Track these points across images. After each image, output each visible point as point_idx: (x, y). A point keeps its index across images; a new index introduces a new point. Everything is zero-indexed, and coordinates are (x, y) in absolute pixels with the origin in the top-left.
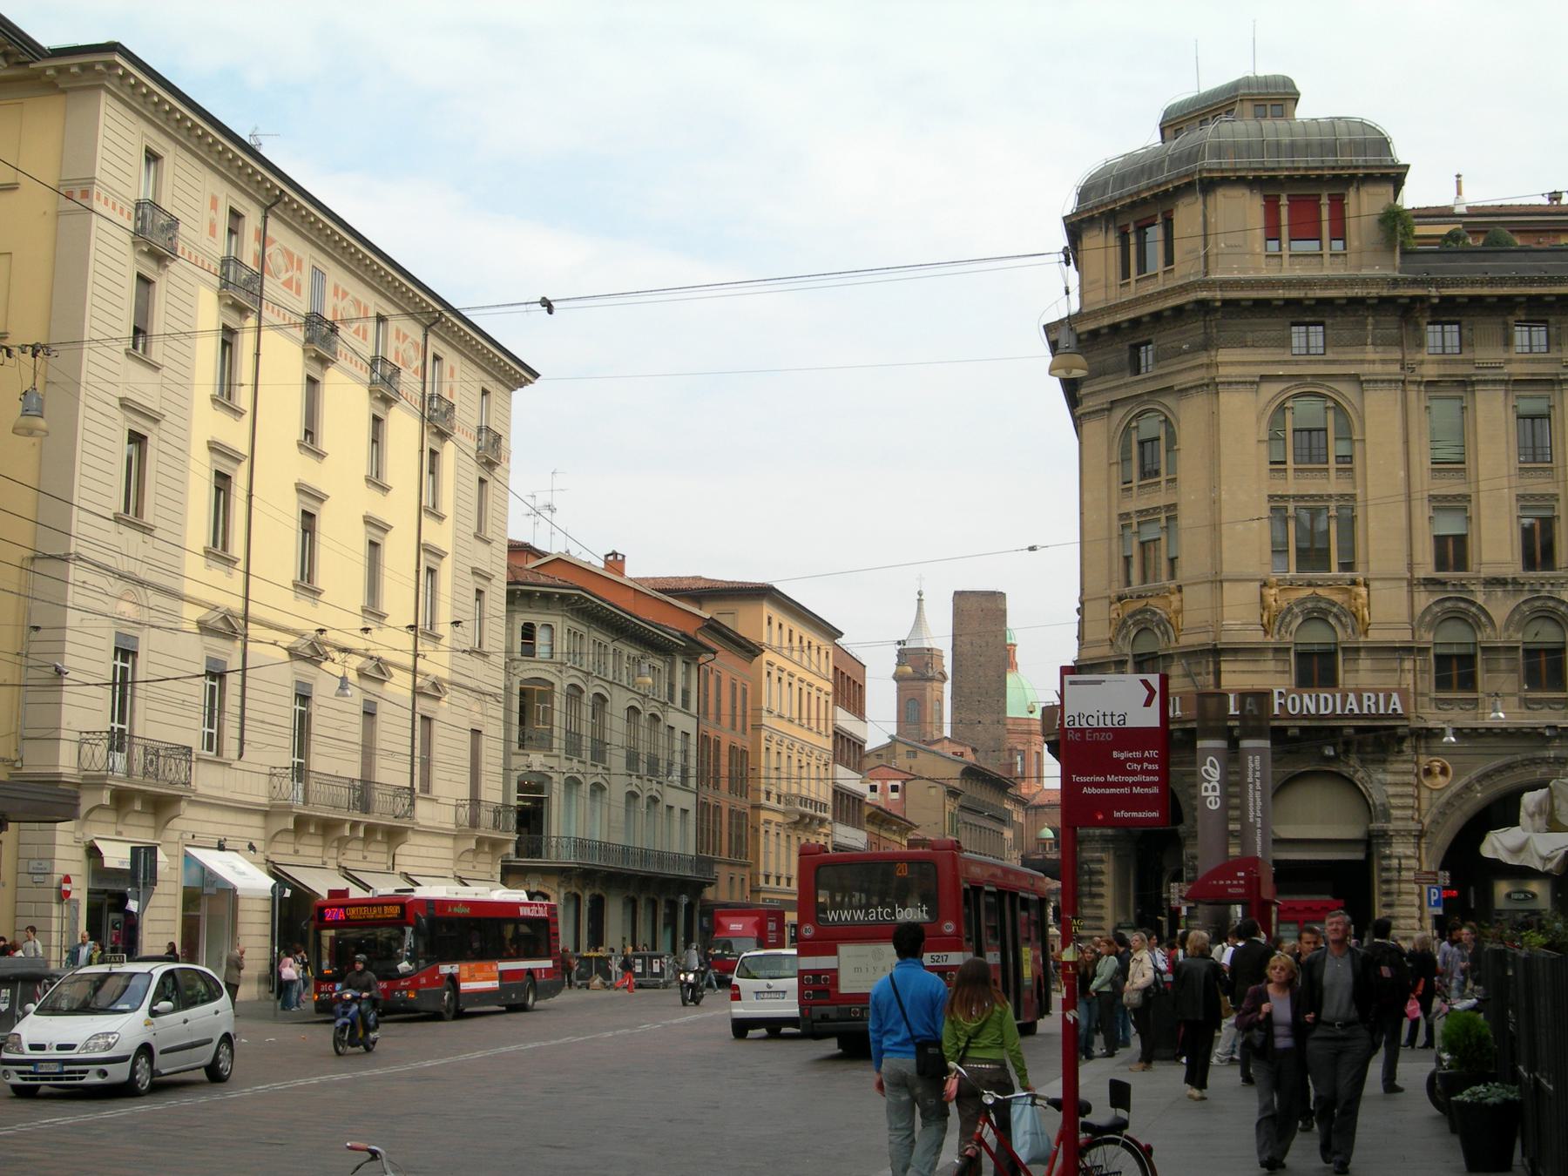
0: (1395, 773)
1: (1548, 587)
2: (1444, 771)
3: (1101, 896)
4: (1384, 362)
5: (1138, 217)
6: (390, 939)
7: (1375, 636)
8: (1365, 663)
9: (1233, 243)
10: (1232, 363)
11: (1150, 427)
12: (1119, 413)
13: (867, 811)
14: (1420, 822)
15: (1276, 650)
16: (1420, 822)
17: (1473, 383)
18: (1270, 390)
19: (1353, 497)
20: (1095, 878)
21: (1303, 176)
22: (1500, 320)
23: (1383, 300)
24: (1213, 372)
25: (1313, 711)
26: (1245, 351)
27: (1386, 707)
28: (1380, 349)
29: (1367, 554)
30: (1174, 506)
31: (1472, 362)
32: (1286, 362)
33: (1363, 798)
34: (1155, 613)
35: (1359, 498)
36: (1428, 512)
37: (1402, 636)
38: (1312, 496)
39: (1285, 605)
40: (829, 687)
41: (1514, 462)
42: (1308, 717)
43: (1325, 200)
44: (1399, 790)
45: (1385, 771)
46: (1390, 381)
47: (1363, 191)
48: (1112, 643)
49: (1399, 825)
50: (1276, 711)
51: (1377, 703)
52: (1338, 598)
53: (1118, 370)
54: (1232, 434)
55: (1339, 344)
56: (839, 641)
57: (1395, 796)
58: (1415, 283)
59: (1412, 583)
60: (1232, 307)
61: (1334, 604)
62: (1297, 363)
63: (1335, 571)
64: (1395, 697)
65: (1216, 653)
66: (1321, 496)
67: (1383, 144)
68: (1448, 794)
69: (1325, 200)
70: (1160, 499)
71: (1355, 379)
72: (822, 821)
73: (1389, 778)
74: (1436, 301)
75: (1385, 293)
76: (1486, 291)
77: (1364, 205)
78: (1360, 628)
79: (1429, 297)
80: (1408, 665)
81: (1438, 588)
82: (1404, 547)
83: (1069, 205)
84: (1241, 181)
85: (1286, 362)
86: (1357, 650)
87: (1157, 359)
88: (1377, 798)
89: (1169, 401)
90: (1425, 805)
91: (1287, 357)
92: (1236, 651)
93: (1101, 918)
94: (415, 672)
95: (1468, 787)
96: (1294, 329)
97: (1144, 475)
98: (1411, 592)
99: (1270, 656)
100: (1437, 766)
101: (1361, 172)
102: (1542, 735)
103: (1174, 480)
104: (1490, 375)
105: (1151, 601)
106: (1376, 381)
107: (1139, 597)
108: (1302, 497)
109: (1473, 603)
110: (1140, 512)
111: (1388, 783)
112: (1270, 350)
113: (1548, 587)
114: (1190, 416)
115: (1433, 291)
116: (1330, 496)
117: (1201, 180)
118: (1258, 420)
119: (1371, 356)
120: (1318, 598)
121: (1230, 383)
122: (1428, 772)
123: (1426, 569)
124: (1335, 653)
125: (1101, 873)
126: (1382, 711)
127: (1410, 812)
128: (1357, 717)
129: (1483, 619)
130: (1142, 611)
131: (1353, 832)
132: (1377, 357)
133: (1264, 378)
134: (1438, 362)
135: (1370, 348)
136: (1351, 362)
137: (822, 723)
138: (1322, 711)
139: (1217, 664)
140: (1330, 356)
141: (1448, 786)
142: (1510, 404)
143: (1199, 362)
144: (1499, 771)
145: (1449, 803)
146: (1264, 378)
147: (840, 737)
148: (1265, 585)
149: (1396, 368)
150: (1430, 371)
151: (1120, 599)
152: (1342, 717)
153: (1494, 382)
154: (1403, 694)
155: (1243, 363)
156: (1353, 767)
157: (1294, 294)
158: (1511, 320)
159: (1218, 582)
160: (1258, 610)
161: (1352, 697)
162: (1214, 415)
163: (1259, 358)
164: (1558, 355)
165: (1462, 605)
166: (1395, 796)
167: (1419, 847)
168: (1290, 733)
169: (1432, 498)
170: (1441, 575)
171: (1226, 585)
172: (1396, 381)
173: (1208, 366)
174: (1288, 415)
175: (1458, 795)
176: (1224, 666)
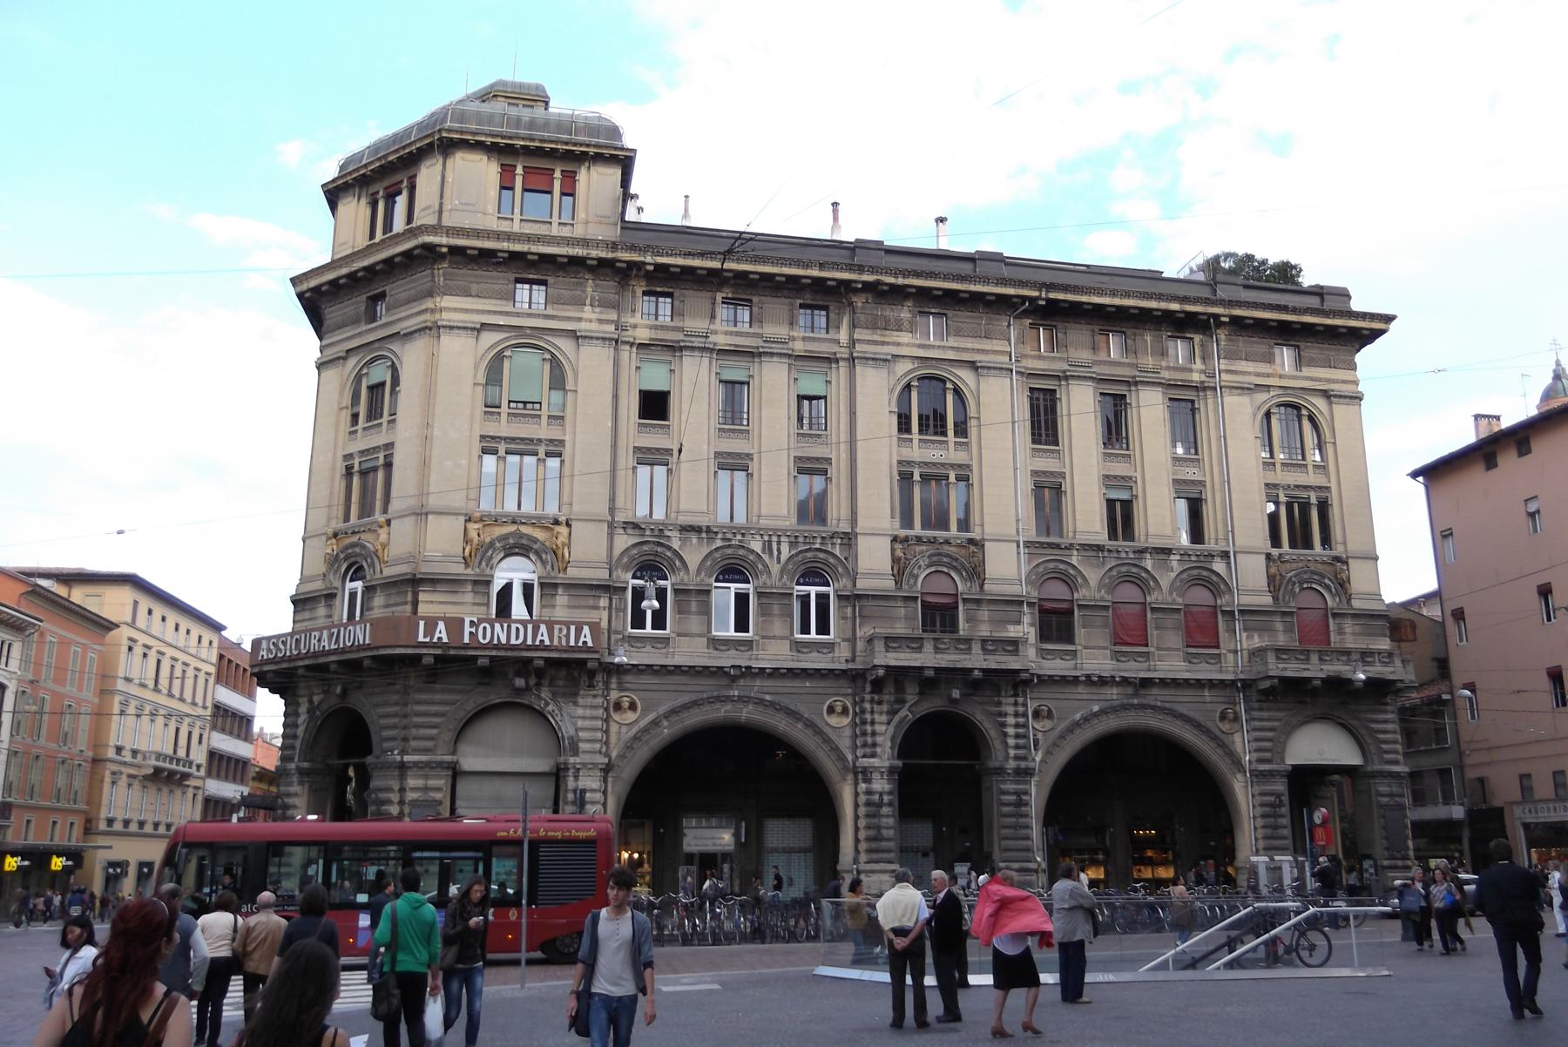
0: (585, 707)
1: (739, 537)
2: (633, 707)
4: (600, 321)
5: (386, 183)
7: (572, 572)
8: (562, 599)
9: (465, 194)
10: (455, 310)
11: (380, 373)
14: (607, 755)
15: (475, 582)
16: (607, 755)
17: (681, 349)
18: (489, 338)
19: (562, 442)
23: (602, 262)
24: (437, 316)
25: (504, 641)
26: (470, 299)
27: (577, 640)
29: (571, 496)
30: (392, 444)
31: (681, 329)
32: (507, 314)
33: (554, 731)
34: (364, 547)
35: (568, 445)
36: (631, 462)
37: (602, 575)
38: (522, 439)
39: (488, 540)
40: (212, 670)
41: (714, 424)
42: (499, 647)
43: (558, 174)
44: (588, 723)
45: (575, 704)
46: (604, 339)
49: (586, 758)
50: (466, 640)
51: (568, 636)
52: (539, 535)
53: (356, 321)
54: (447, 360)
58: (633, 248)
59: (611, 526)
61: (535, 541)
62: (518, 315)
63: (649, 629)
64: (586, 630)
65: (415, 583)
66: (531, 440)
67: (615, 132)
68: (635, 729)
69: (558, 174)
70: (379, 439)
71: (574, 335)
73: (580, 711)
74: (651, 268)
75: (603, 255)
76: (696, 263)
77: (596, 182)
79: (644, 263)
80: (604, 602)
81: (637, 532)
82: (606, 491)
85: (507, 314)
86: (555, 586)
87: (388, 309)
88: (567, 730)
89: (395, 347)
90: (613, 739)
91: (509, 308)
92: (433, 581)
95: (655, 723)
97: (370, 418)
98: (611, 536)
99: (470, 588)
100: (625, 703)
101: (592, 150)
102: (727, 674)
105: (363, 536)
107: (354, 533)
108: (513, 439)
109: (669, 548)
110: (362, 453)
111: (579, 718)
113: (739, 537)
114: (411, 358)
115: (649, 259)
116: (540, 440)
117: (441, 139)
119: (585, 315)
120: (522, 536)
121: (451, 328)
122: (618, 707)
124: (1070, 612)
125: (295, 807)
126: (572, 643)
127: (598, 746)
128: (547, 648)
130: (353, 545)
131: (542, 765)
132: (594, 316)
134: (651, 327)
135: (588, 308)
136: (569, 319)
137: (177, 683)
138: (513, 641)
139: (415, 595)
140: (550, 311)
142: (714, 370)
143: (423, 307)
144: (686, 707)
145: (635, 738)
146: (484, 326)
148: (469, 520)
149: (612, 328)
150: (643, 335)
151: (335, 535)
152: (534, 648)
154: (595, 628)
156: (544, 698)
157: (518, 247)
159: (421, 514)
160: (461, 544)
161: (543, 628)
163: (481, 307)
167: (605, 781)
168: (480, 662)
169: (637, 449)
172: (610, 339)
174: (506, 363)
175: (645, 730)
176: (422, 597)
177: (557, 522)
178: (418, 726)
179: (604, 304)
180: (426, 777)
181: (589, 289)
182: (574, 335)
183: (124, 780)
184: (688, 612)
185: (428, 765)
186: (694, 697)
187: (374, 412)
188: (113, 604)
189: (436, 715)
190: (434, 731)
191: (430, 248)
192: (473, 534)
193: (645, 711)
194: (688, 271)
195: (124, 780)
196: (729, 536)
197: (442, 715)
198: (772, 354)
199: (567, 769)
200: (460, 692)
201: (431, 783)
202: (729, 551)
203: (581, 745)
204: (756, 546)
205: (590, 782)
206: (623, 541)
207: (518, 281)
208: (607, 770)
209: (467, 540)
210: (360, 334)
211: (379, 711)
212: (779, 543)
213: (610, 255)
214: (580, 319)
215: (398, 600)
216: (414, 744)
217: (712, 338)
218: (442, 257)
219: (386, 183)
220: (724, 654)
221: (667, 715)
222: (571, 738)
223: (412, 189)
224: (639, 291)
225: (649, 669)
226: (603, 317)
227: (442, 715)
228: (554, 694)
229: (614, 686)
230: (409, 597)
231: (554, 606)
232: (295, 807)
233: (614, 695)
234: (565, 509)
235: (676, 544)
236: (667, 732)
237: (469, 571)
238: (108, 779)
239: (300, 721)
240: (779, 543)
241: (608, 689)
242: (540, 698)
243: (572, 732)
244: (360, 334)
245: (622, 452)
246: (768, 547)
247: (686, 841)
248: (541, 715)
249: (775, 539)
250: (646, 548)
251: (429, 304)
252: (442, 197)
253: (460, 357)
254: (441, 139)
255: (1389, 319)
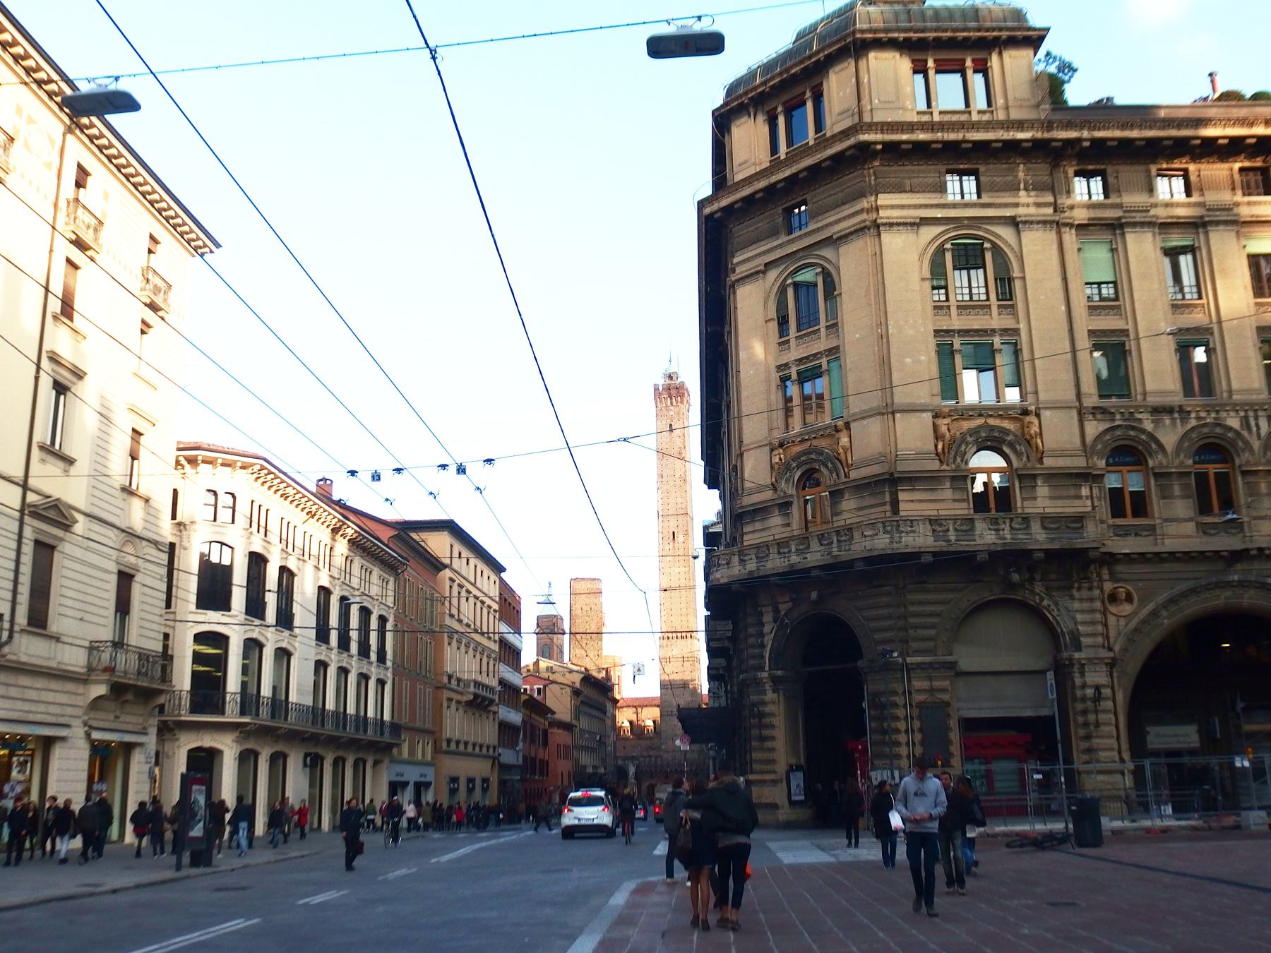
0: (1081, 600)
1: (1213, 415)
2: (1129, 598)
3: (773, 738)
4: (1038, 205)
5: (785, 97)
6: (417, 802)
8: (1042, 491)
9: (895, 91)
10: (892, 207)
12: (772, 275)
13: (524, 697)
14: (1110, 649)
15: (953, 479)
18: (929, 232)
20: (766, 720)
21: (951, 39)
22: (1142, 168)
26: (903, 195)
28: (1033, 193)
31: (1120, 206)
44: (1087, 617)
45: (1072, 597)
47: (1006, 54)
48: (774, 487)
53: (774, 233)
55: (994, 189)
56: (502, 575)
57: (1083, 623)
60: (893, 151)
66: (985, 331)
67: (1018, 15)
71: (1014, 222)
72: (492, 701)
73: (1077, 605)
74: (1086, 144)
78: (1033, 455)
80: (1085, 491)
81: (1108, 417)
82: (1071, 376)
83: (719, 100)
84: (892, 44)
86: (1034, 477)
88: (1065, 625)
89: (827, 252)
90: (1112, 633)
93: (773, 761)
94: (25, 487)
95: (1155, 613)
96: (949, 177)
99: (948, 484)
100: (1122, 593)
101: (1005, 34)
103: (836, 325)
104: (1138, 217)
106: (1032, 222)
109: (1143, 431)
110: (800, 361)
111: (1076, 612)
112: (928, 195)
114: (850, 262)
115: (1086, 134)
116: (993, 331)
117: (855, 41)
118: (921, 259)
120: (992, 428)
121: (891, 225)
122: (1113, 598)
123: (1092, 400)
125: (773, 715)
129: (1154, 446)
132: (1031, 200)
133: (926, 221)
135: (1022, 193)
136: (1006, 205)
141: (1134, 613)
143: (858, 208)
144: (1184, 595)
146: (926, 221)
147: (503, 643)
148: (936, 416)
149: (1050, 210)
150: (1081, 216)
151: (781, 445)
153: (1142, 224)
155: (903, 207)
156: (1038, 593)
157: (952, 136)
158: (1153, 169)
162: (879, 255)
164: (1118, 201)
165: (1132, 433)
166: (1083, 623)
170: (1105, 403)
171: (898, 416)
172: (1051, 222)
173: (868, 211)
175: (1145, 621)
176: (902, 496)
177: (1025, 412)
178: (916, 627)
179: (1038, 188)
180: (930, 679)
181: (1021, 174)
182: (1014, 222)
183: (454, 705)
184: (1172, 497)
185: (930, 665)
186: (1191, 584)
187: (807, 321)
188: (438, 544)
189: (931, 615)
190: (932, 632)
191: (864, 147)
192: (944, 429)
193: (1143, 601)
194: (1126, 143)
195: (454, 705)
196: (1203, 414)
197: (938, 615)
198: (1218, 223)
199: (1072, 665)
200: (953, 590)
201: (936, 684)
202: (1206, 430)
203: (1082, 639)
204: (1234, 422)
205: (1098, 677)
206: (1094, 428)
207: (949, 172)
208: (1112, 664)
209: (938, 436)
210: (780, 246)
211: (867, 615)
212: (1256, 418)
213: (1046, 135)
214: (1017, 205)
215: (873, 501)
216: (914, 645)
217: (1152, 212)
218: (875, 154)
219: (785, 97)
220: (1214, 539)
221: (1165, 606)
222: (1071, 633)
223: (818, 97)
224: (1071, 171)
225: (1142, 558)
226: (1041, 200)
227: (938, 615)
228: (1047, 588)
229: (1106, 577)
230: (887, 498)
231: (1035, 499)
232: (773, 715)
233: (1108, 586)
234: (1031, 398)
235: (1148, 426)
236: (1167, 622)
237: (944, 467)
238: (445, 704)
239: (767, 629)
240: (1256, 418)
241: (1101, 580)
242: (1033, 592)
243: (1071, 625)
244: (780, 246)
245: (1077, 336)
246: (1245, 421)
247: (1149, 738)
248: (1037, 613)
249: (1251, 414)
250: (1118, 433)
251: (865, 203)
252: (859, 101)
253: (905, 254)
254: (855, 41)
255: (218, 246)
